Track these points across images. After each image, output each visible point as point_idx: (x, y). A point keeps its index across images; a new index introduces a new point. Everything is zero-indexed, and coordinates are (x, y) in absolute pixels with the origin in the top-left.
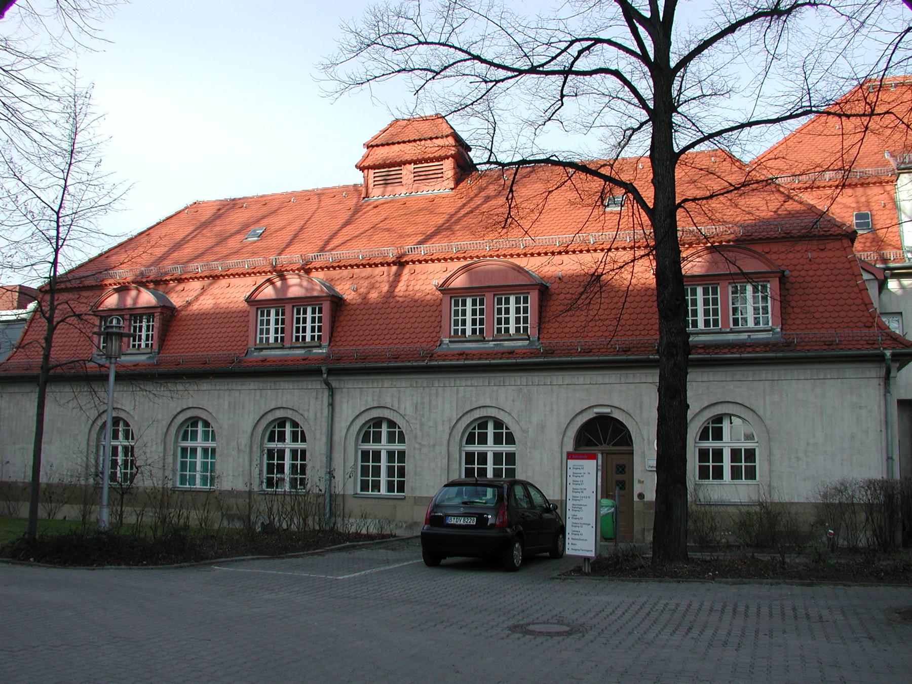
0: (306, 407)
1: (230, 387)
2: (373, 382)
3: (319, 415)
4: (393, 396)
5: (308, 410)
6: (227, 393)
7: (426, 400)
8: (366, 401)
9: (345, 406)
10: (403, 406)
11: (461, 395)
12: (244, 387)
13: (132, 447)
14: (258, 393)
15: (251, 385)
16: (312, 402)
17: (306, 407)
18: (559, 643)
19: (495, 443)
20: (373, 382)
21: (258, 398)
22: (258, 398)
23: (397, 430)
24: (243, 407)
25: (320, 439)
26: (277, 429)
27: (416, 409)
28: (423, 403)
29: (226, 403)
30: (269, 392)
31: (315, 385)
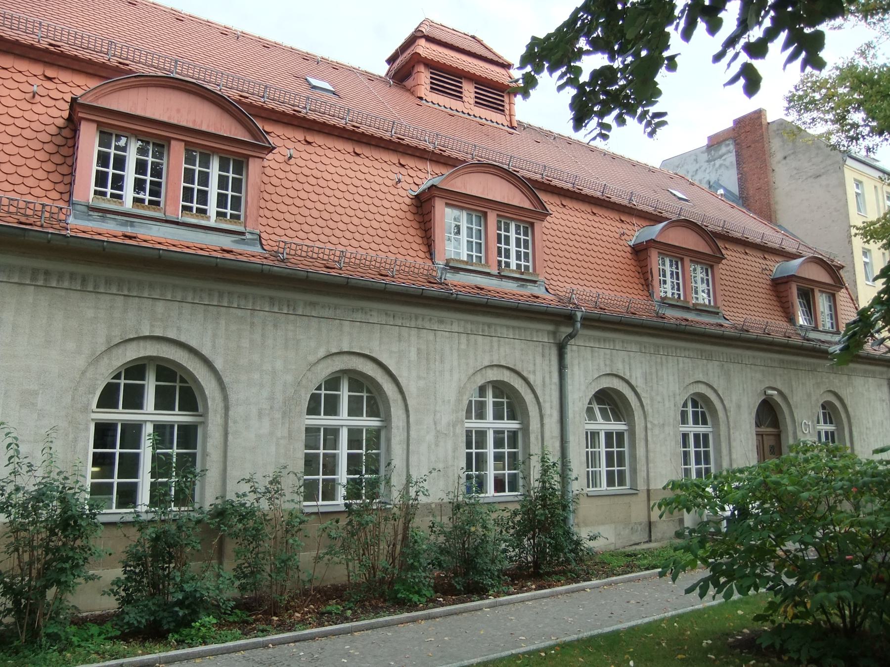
0: (531, 368)
1: (420, 323)
2: (221, 295)
3: (547, 380)
4: (624, 361)
5: (534, 372)
6: (414, 332)
7: (654, 370)
8: (599, 365)
9: (576, 369)
10: (634, 374)
11: (681, 365)
12: (442, 327)
13: (468, 417)
14: (463, 337)
15: (456, 322)
16: (539, 360)
17: (531, 368)
18: (219, 576)
19: (157, 407)
20: (221, 295)
21: (463, 347)
22: (463, 347)
23: (178, 385)
24: (442, 362)
25: (551, 415)
26: (122, 382)
27: (646, 379)
28: (651, 374)
29: (413, 351)
30: (480, 338)
31: (542, 334)
